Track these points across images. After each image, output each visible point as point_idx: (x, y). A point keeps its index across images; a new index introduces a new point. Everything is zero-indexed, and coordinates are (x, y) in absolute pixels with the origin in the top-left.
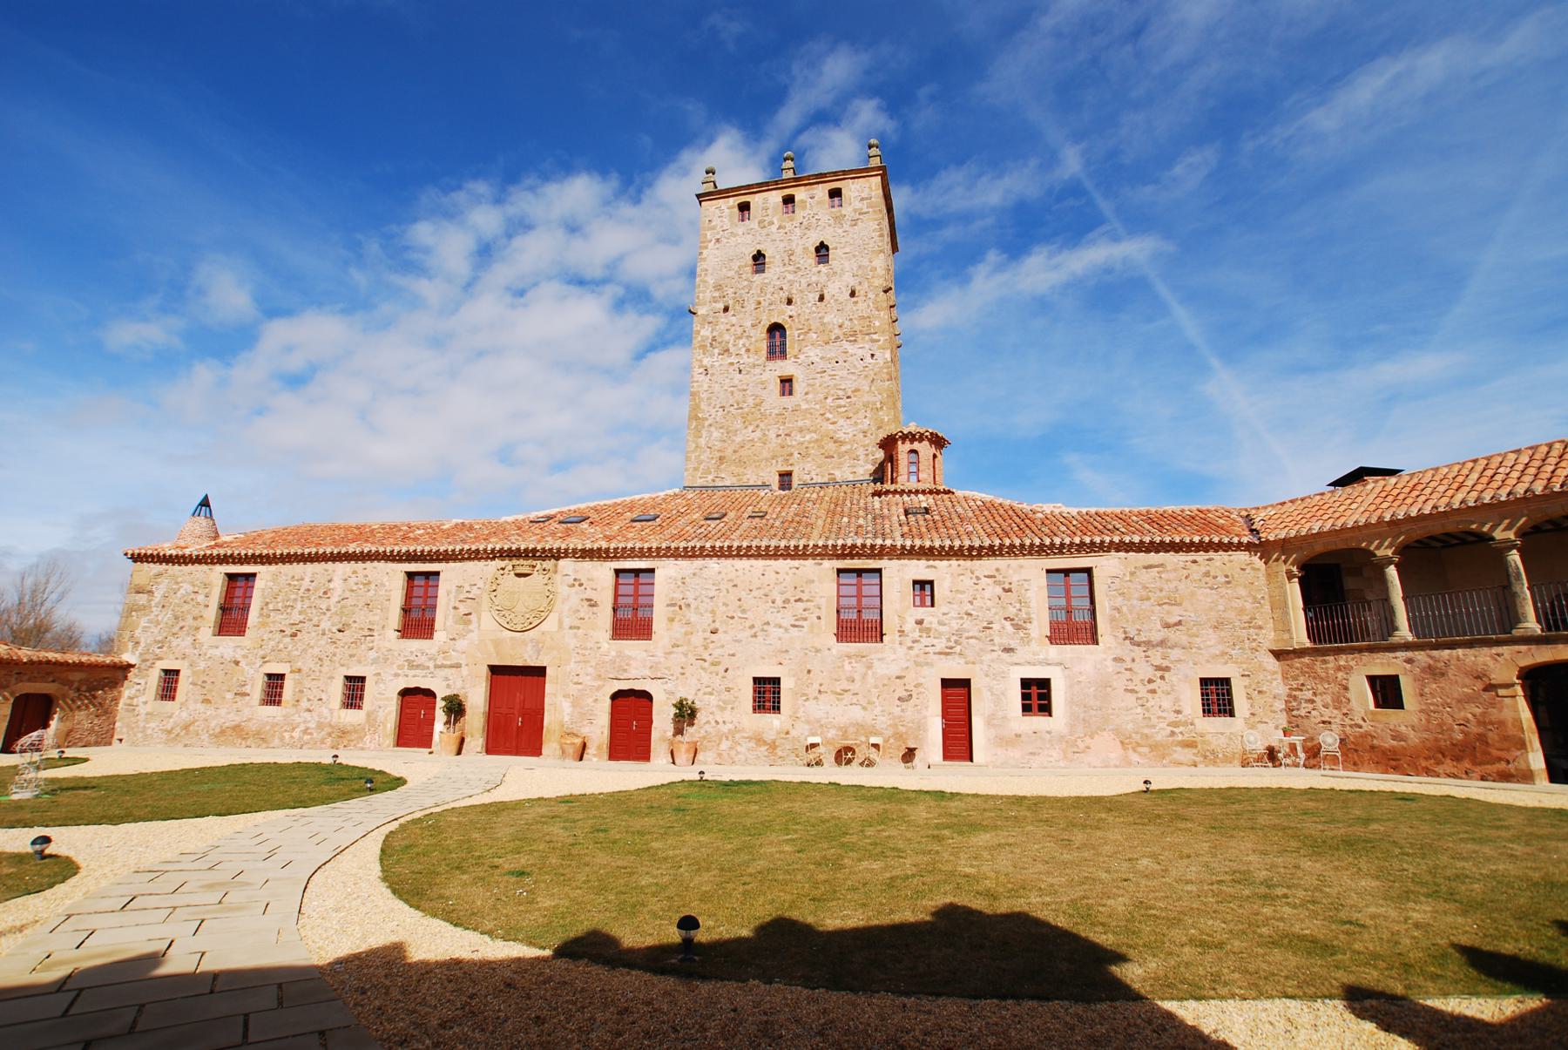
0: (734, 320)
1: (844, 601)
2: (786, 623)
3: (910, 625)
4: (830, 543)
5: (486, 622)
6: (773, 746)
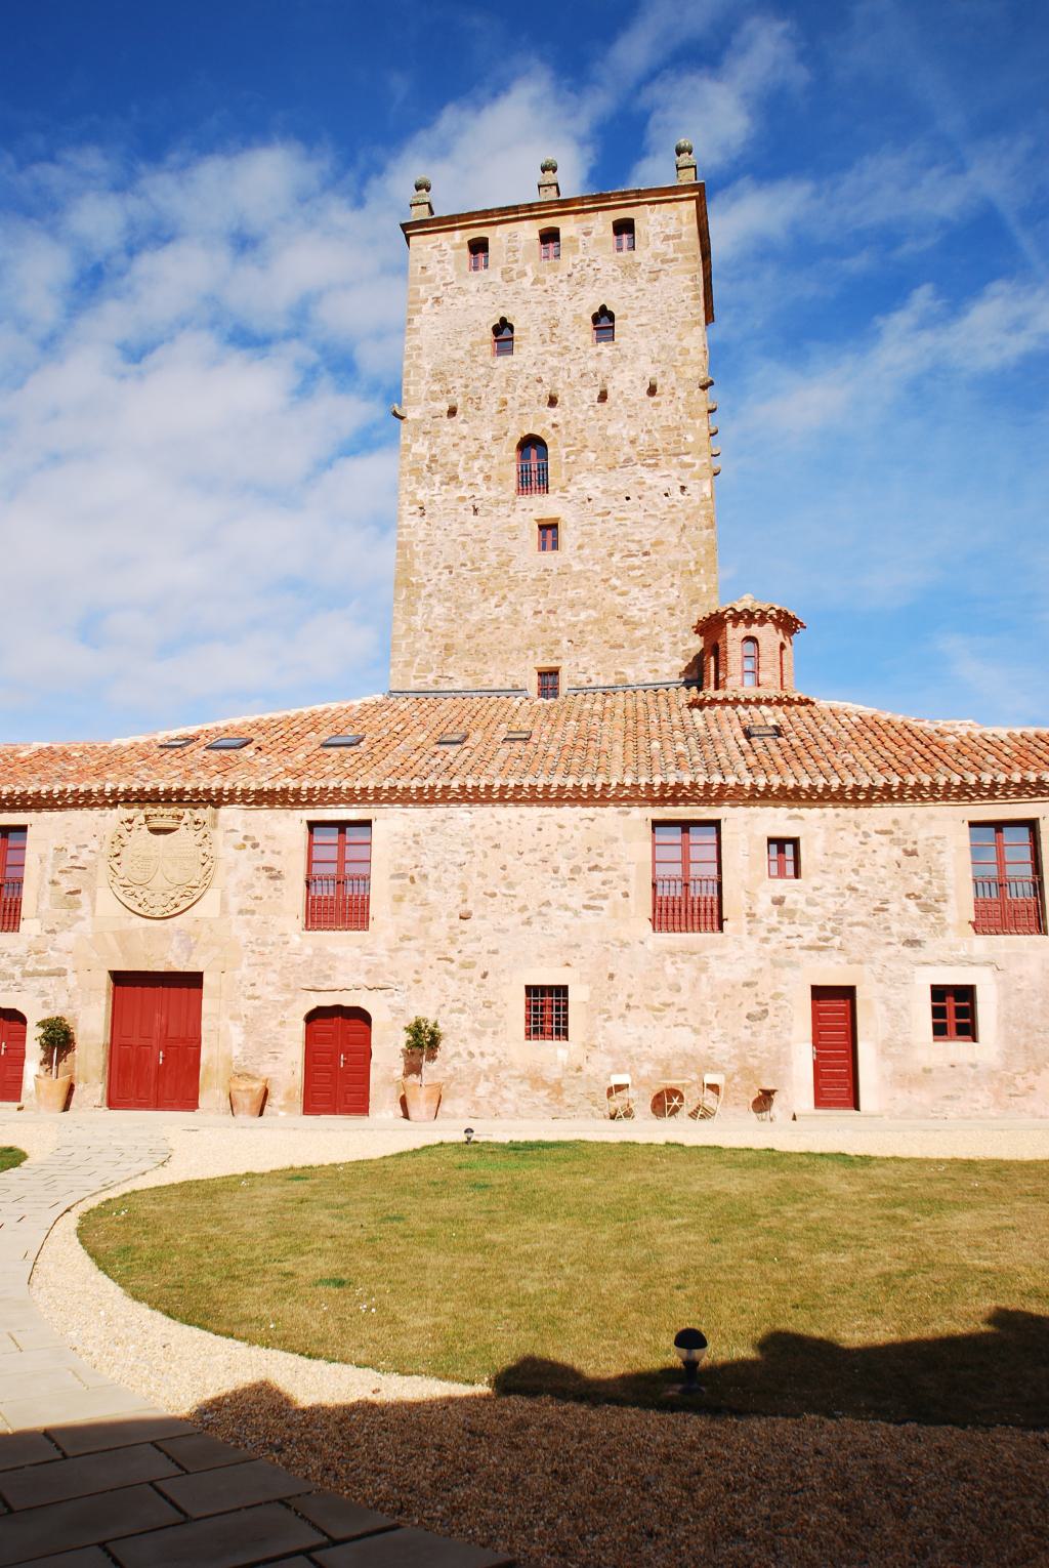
0: (465, 429)
1: (662, 870)
2: (576, 902)
3: (764, 905)
4: (643, 781)
5: (105, 905)
6: (557, 1089)
